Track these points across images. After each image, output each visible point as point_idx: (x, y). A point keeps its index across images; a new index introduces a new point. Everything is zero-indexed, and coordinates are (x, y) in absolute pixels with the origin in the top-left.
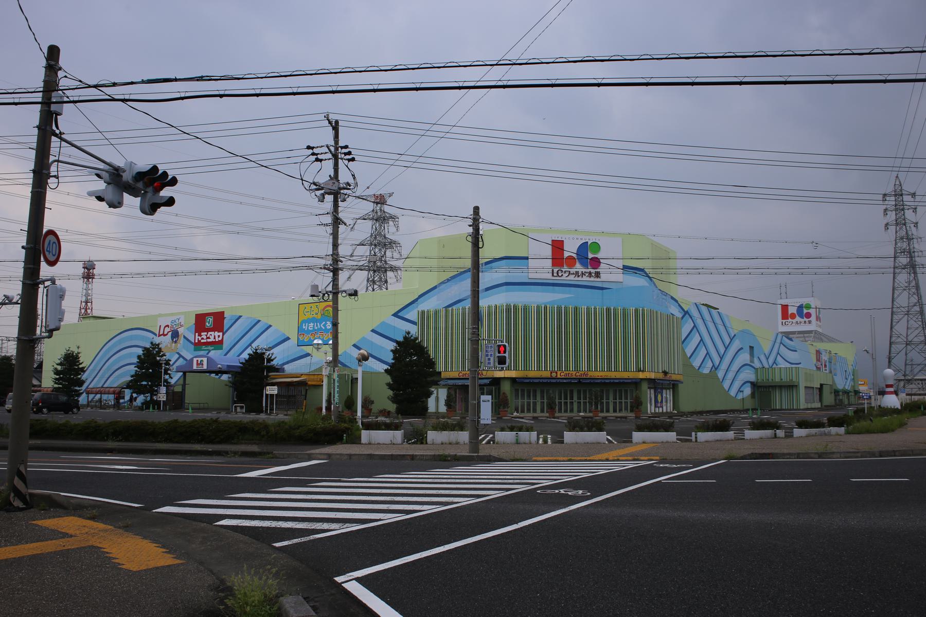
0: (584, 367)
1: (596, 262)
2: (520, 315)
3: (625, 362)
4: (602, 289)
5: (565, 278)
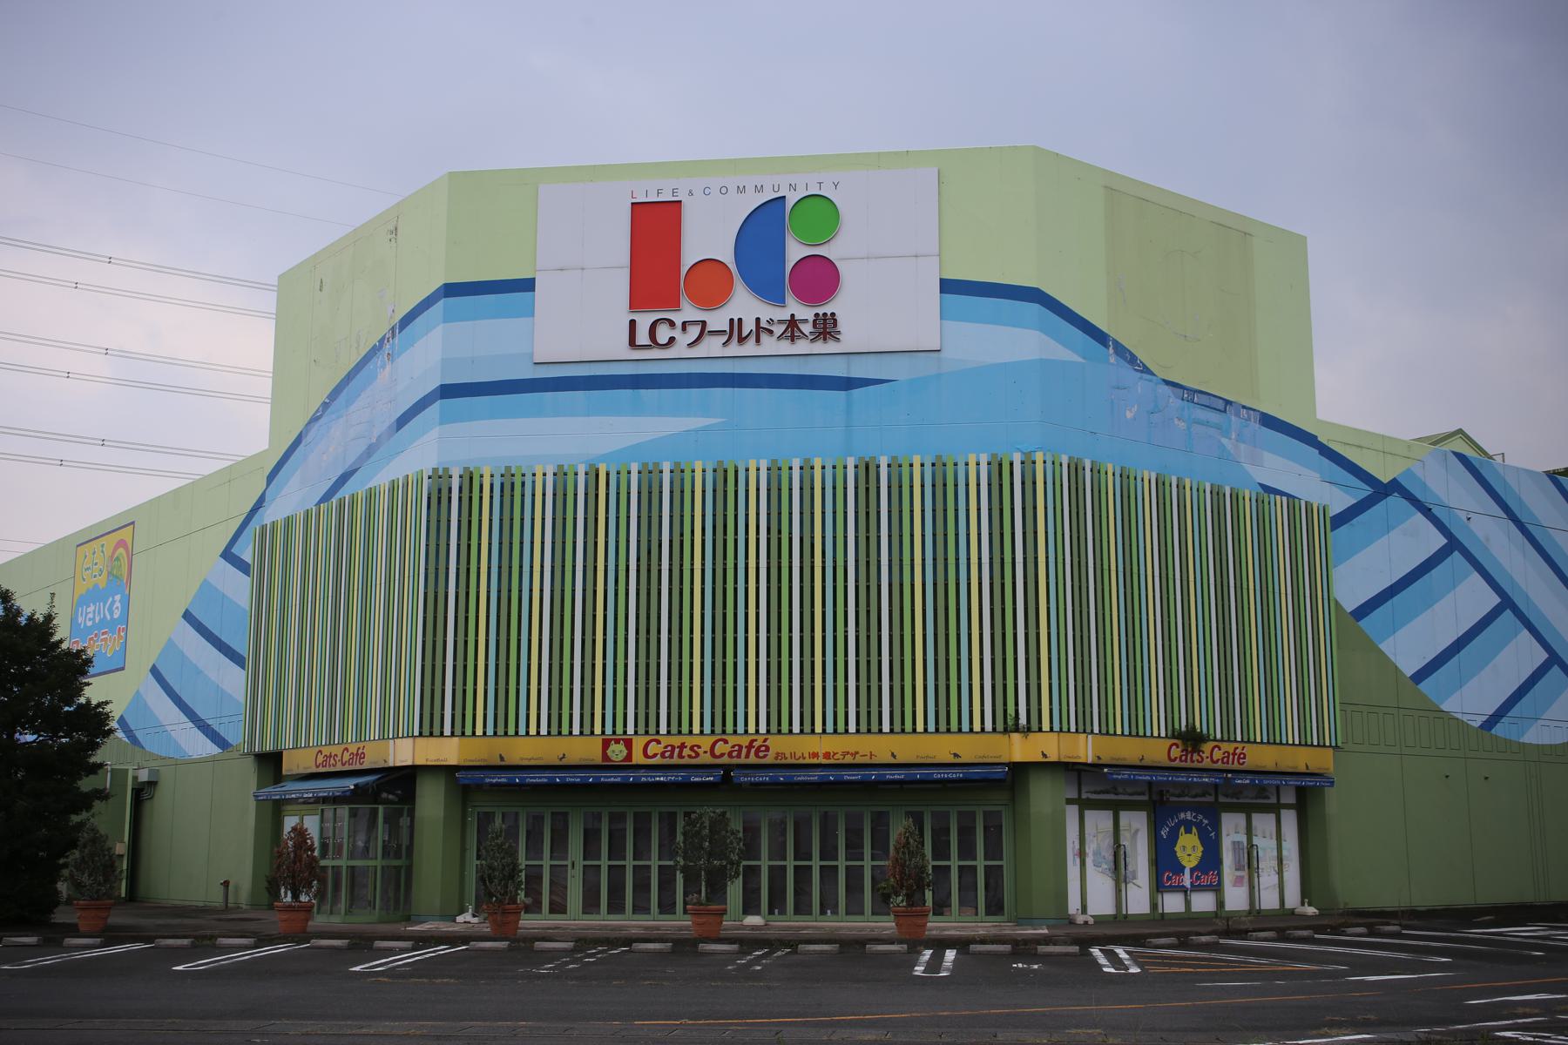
0: (754, 713)
1: (819, 279)
2: (487, 514)
3: (502, 696)
4: (848, 384)
5: (683, 354)
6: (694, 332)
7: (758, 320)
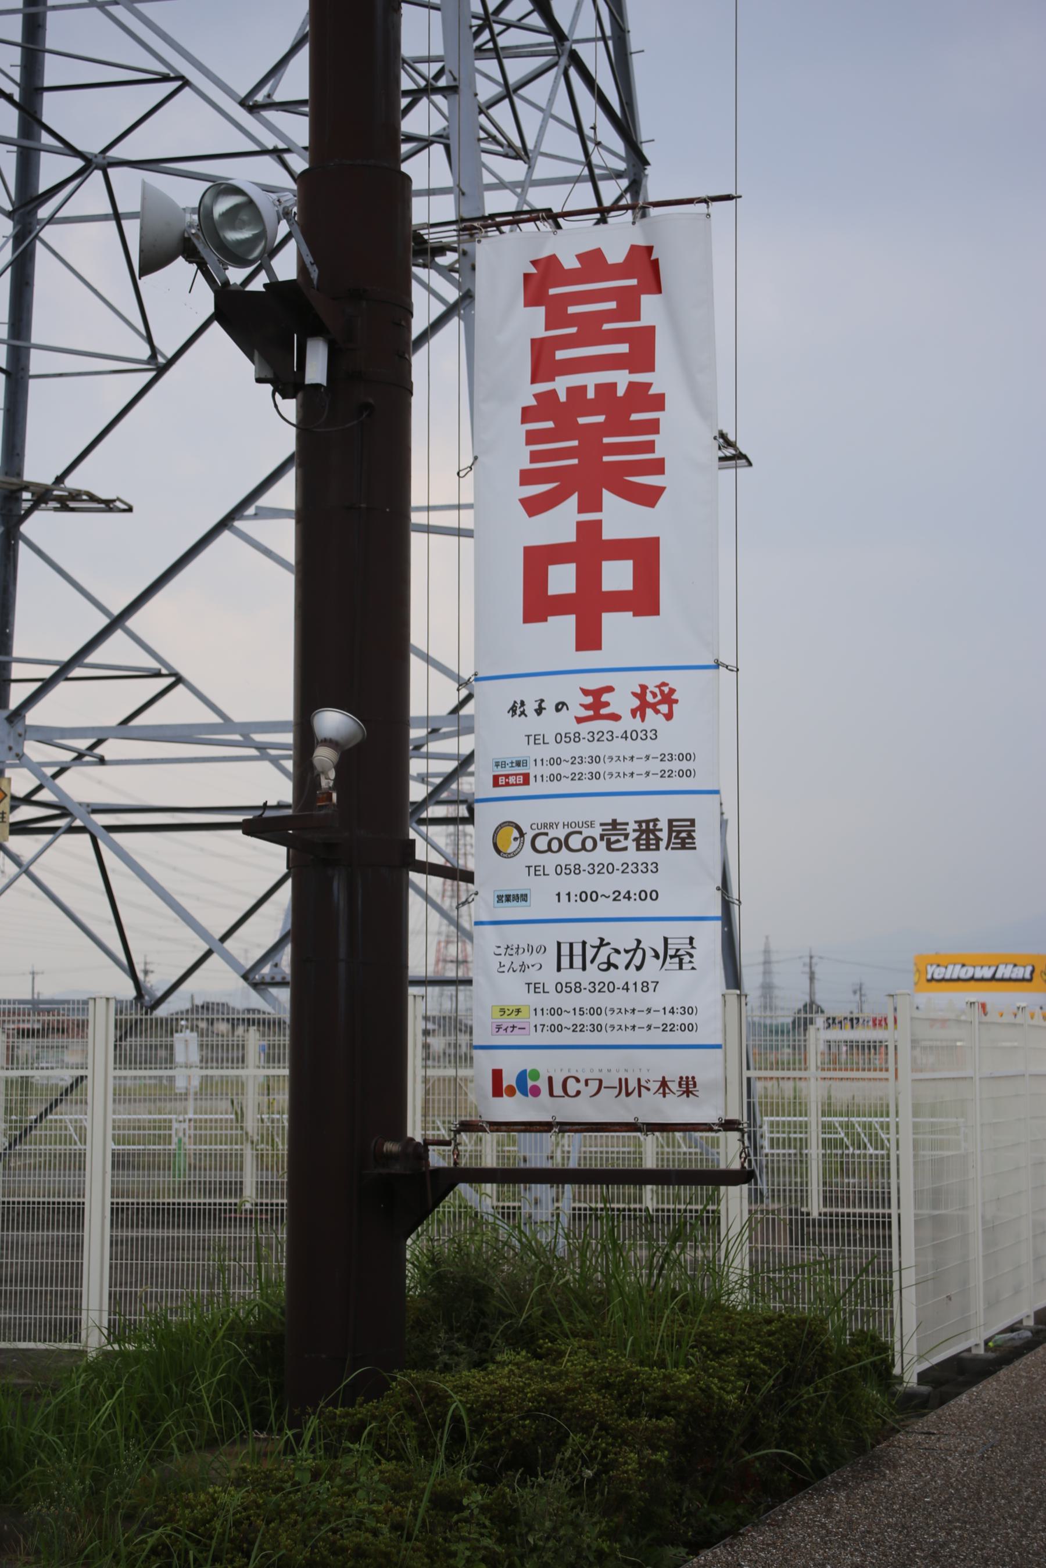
6: (594, 1085)
7: (639, 1080)
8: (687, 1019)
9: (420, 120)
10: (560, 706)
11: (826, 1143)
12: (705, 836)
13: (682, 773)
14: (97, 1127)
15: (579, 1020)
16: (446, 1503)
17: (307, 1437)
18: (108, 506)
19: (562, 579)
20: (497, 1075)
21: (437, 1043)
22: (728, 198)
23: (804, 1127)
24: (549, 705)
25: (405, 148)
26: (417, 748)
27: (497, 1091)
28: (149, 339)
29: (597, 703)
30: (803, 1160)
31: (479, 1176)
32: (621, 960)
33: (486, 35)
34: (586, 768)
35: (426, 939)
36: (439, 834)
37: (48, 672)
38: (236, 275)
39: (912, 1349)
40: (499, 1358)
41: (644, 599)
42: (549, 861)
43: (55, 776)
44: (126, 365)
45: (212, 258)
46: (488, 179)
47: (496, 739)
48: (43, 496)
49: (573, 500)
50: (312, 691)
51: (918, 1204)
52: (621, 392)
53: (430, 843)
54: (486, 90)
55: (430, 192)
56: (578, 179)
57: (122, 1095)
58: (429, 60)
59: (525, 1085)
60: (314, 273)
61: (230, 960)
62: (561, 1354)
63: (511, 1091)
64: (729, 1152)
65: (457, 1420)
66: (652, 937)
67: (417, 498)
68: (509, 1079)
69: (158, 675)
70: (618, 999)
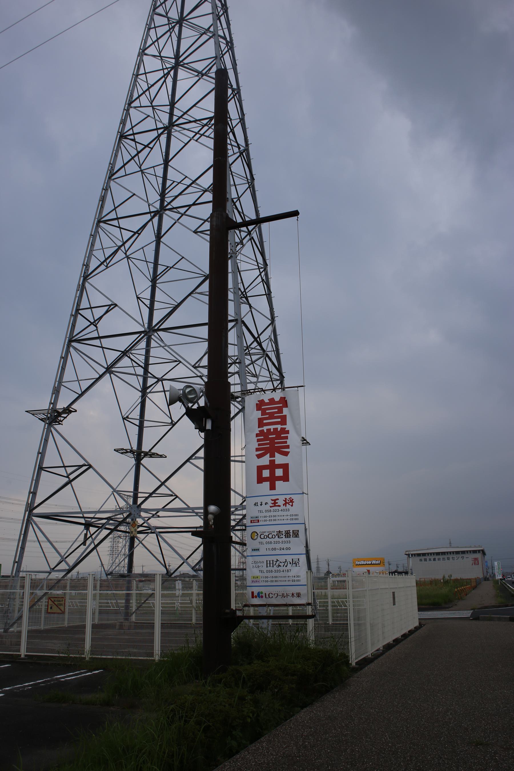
8: (298, 579)
9: (232, 369)
10: (266, 504)
11: (333, 606)
12: (301, 534)
13: (295, 519)
14: (158, 604)
15: (272, 579)
16: (242, 699)
17: (208, 682)
18: (161, 456)
19: (266, 473)
20: (253, 593)
21: (239, 583)
22: (302, 386)
23: (327, 602)
24: (264, 503)
25: (229, 375)
26: (233, 513)
27: (253, 597)
28: (171, 418)
29: (275, 503)
30: (327, 610)
31: (249, 618)
32: (282, 564)
33: (247, 351)
34: (272, 518)
35: (235, 558)
36: (239, 533)
37: (147, 495)
38: (190, 405)
39: (354, 657)
40: (254, 662)
41: (285, 478)
42: (264, 541)
43: (148, 520)
44: (165, 424)
45: (185, 401)
46: (248, 381)
47: (251, 511)
48: (146, 454)
49: (268, 455)
50: (208, 500)
51: (354, 620)
52: (279, 430)
53: (236, 536)
54: (247, 362)
55: (235, 384)
56: (269, 381)
57: (163, 596)
58: (234, 356)
59: (260, 595)
60: (208, 404)
61: (189, 564)
62: (269, 661)
63: (256, 597)
64: (309, 611)
65: (244, 678)
66: (289, 559)
67: (232, 454)
68: (255, 594)
69: (172, 496)
70: (282, 574)
